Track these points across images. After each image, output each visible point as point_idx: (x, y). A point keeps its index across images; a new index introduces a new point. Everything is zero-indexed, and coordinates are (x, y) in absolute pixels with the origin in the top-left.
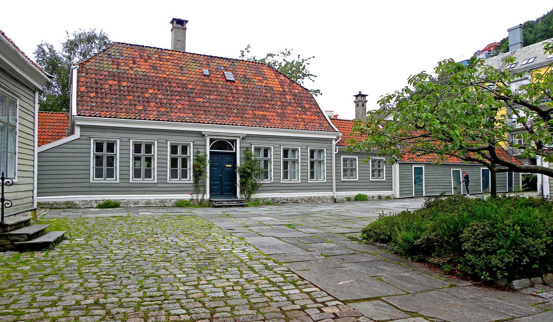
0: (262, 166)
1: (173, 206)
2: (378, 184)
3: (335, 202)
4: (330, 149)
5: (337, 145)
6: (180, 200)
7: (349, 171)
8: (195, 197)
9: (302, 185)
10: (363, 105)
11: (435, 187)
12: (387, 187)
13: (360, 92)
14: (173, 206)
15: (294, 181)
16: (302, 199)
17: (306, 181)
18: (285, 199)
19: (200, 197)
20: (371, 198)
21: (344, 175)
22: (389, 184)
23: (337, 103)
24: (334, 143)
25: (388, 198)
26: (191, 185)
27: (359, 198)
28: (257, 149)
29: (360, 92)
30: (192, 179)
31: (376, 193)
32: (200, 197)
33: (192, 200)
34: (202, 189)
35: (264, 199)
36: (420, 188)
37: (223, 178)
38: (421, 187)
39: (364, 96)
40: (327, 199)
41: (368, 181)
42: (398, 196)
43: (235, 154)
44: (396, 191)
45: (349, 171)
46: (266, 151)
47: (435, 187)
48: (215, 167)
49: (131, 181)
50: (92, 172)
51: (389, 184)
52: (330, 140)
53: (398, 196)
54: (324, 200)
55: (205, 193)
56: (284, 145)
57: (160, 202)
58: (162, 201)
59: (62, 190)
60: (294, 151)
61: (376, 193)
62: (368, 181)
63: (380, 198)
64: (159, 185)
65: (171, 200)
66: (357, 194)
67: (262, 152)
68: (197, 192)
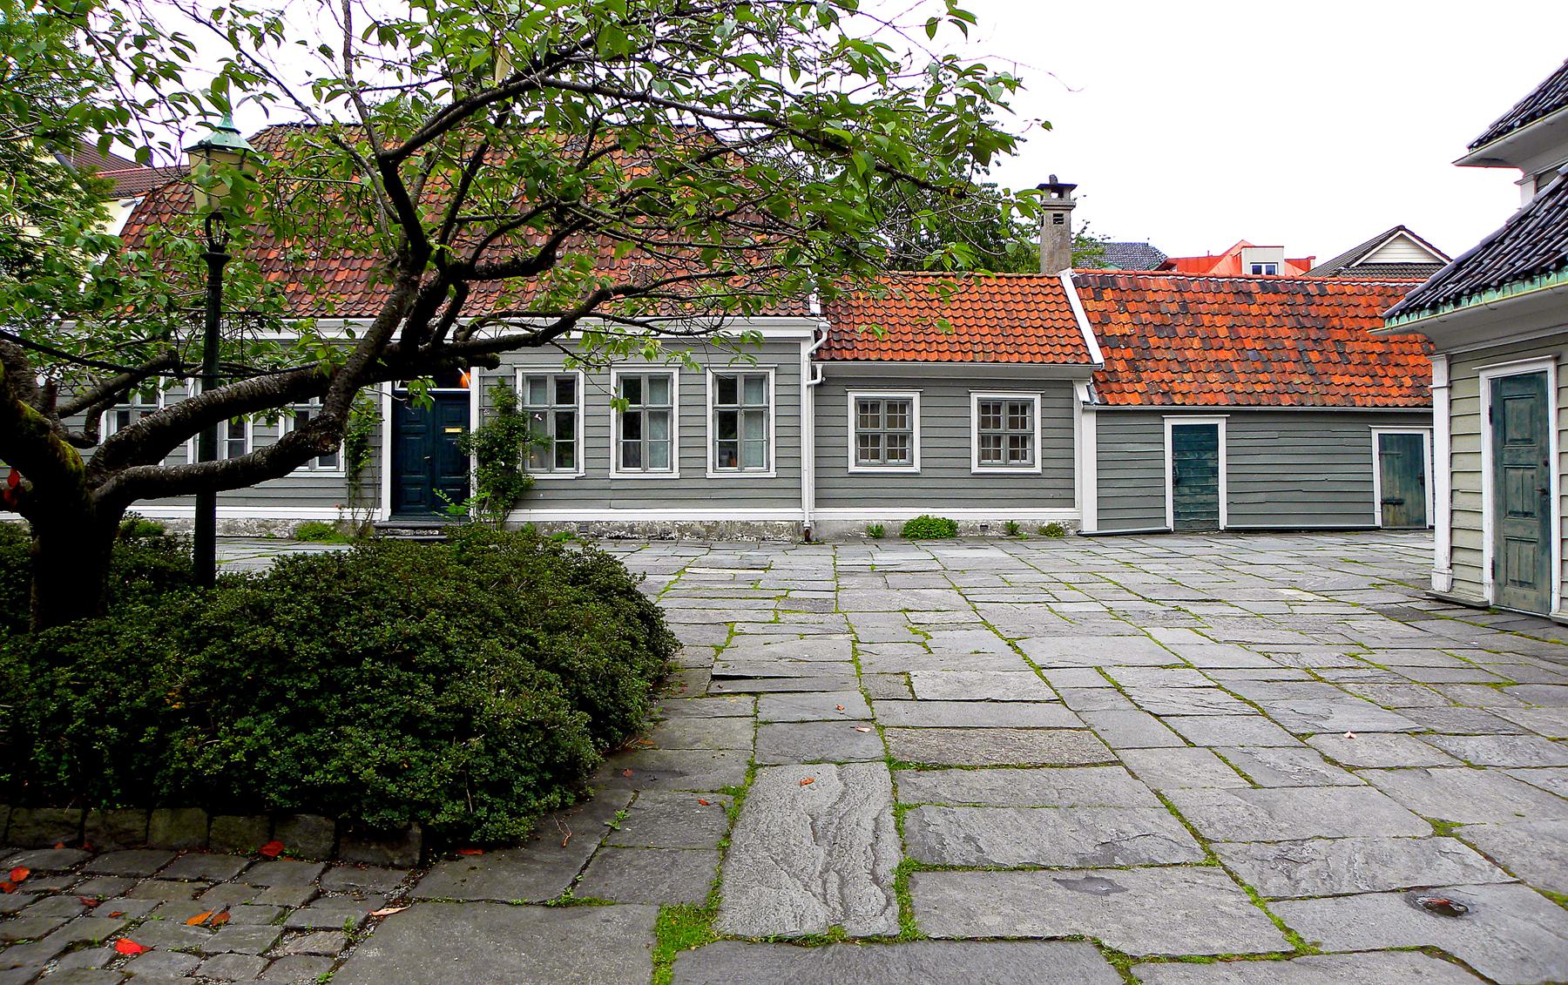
0: (551, 429)
1: (291, 538)
2: (1012, 483)
3: (808, 539)
4: (790, 375)
5: (815, 357)
6: (311, 523)
7: (882, 436)
8: (347, 514)
9: (684, 484)
10: (1058, 219)
11: (1279, 497)
12: (1051, 494)
13: (1053, 178)
14: (291, 538)
15: (657, 473)
16: (682, 529)
17: (696, 474)
18: (622, 527)
19: (362, 515)
20: (973, 530)
21: (984, 455)
22: (792, 483)
23: (1076, 220)
24: (807, 349)
25: (1053, 532)
26: (341, 484)
27: (920, 532)
28: (535, 382)
29: (1053, 178)
30: (342, 468)
31: (998, 515)
32: (362, 515)
33: (340, 522)
34: (368, 493)
35: (555, 525)
36: (1201, 498)
37: (438, 466)
38: (1210, 498)
39: (1061, 189)
40: (776, 529)
41: (964, 473)
42: (1090, 526)
43: (467, 396)
44: (1086, 513)
45: (882, 436)
46: (566, 389)
47: (1279, 497)
48: (416, 434)
49: (710, 474)
50: (711, 453)
51: (792, 483)
52: (795, 343)
53: (1090, 526)
54: (767, 534)
55: (377, 503)
56: (525, 365)
57: (259, 526)
58: (264, 524)
59: (951, 493)
60: (661, 382)
61: (998, 515)
62: (964, 473)
63: (1012, 530)
64: (589, 484)
65: (286, 522)
66: (916, 516)
67: (552, 389)
68: (355, 500)
